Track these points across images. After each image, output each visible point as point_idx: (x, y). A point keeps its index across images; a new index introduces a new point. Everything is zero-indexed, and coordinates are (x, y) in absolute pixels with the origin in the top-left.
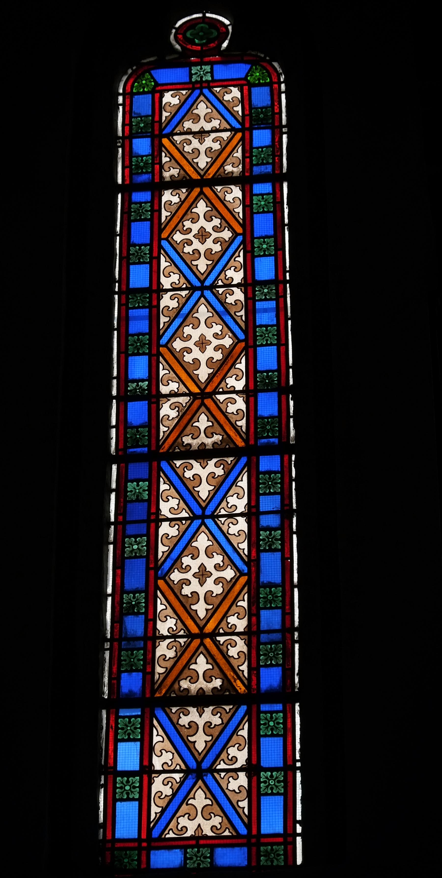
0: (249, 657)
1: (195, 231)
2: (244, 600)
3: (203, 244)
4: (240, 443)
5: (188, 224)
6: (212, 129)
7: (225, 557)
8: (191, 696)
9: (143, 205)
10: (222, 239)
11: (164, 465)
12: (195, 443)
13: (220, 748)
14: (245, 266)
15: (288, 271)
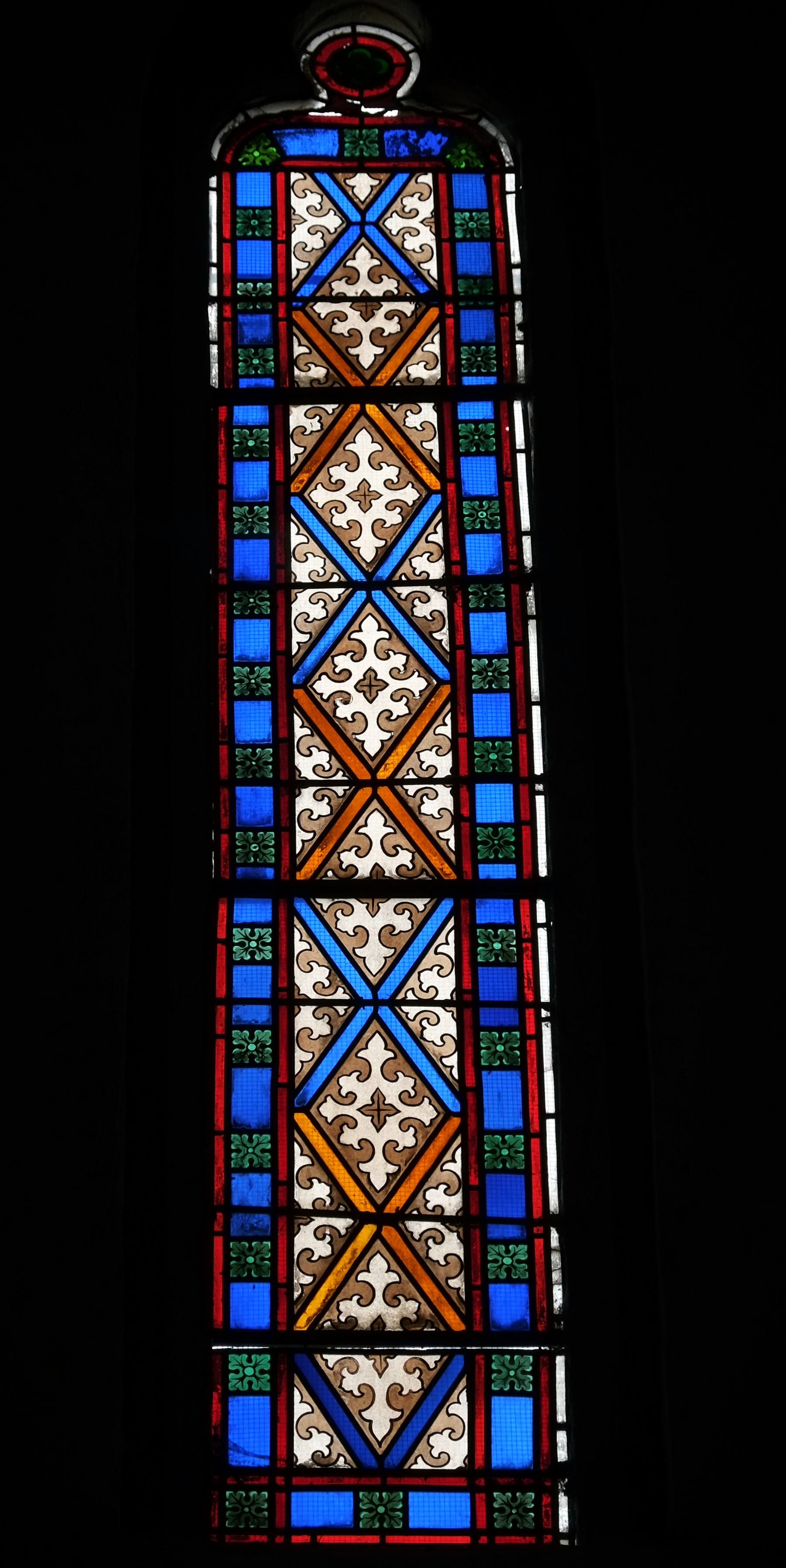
0: (467, 1266)
1: (357, 675)
2: (447, 943)
3: (366, 321)
4: (456, 1323)
5: (343, 662)
6: (385, 293)
7: (419, 1081)
8: (361, 1331)
9: (256, 508)
10: (417, 1123)
11: (302, 907)
12: (365, 1316)
13: (407, 969)
14: (446, 551)
15: (561, 1427)
